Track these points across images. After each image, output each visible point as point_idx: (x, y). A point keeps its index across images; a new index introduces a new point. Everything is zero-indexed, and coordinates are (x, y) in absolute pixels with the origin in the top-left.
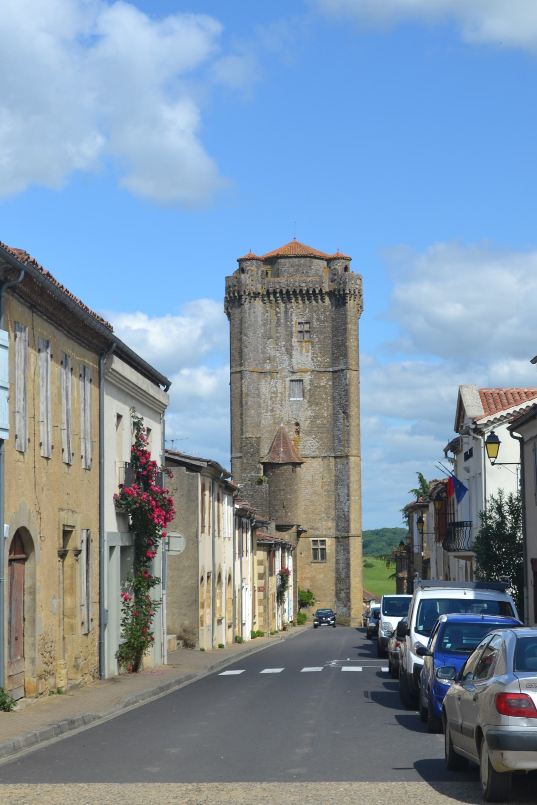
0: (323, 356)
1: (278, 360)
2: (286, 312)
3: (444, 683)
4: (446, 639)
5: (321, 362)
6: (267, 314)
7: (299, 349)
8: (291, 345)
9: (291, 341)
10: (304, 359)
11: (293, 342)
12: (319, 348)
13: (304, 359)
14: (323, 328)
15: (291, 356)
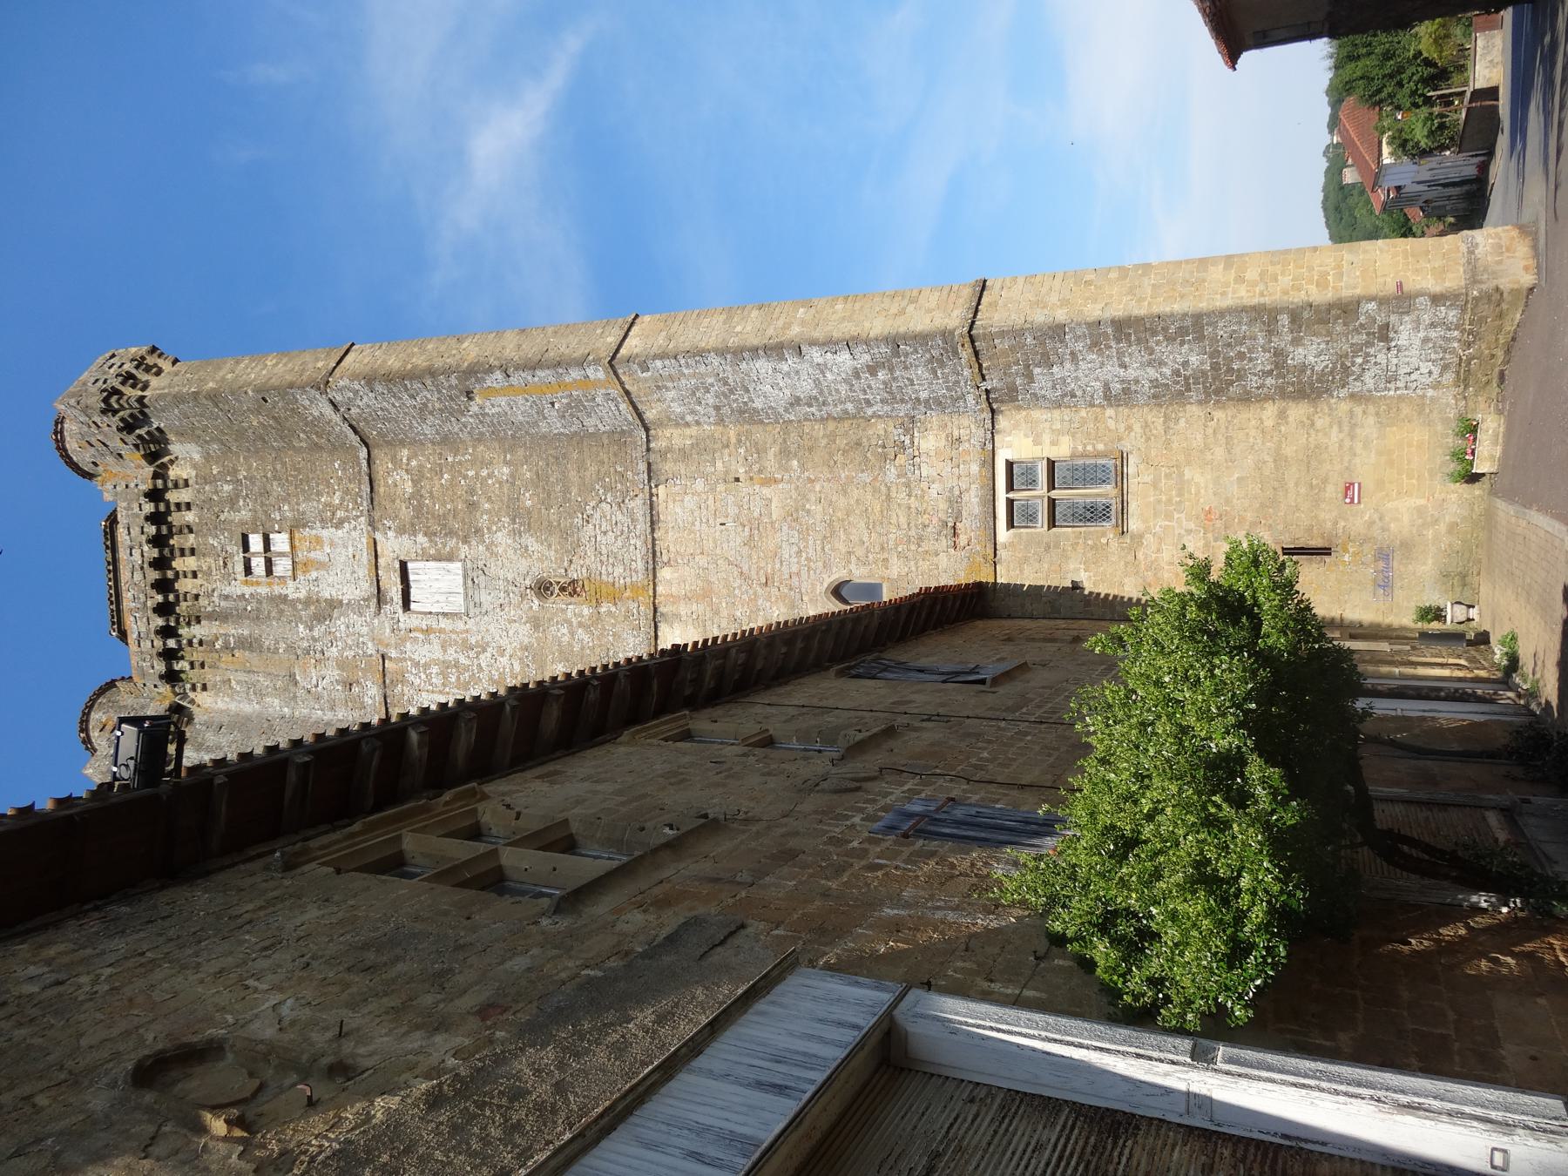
0: (328, 485)
1: (349, 654)
2: (221, 616)
5: (347, 492)
7: (314, 574)
8: (307, 602)
9: (293, 603)
10: (341, 556)
12: (308, 499)
13: (341, 556)
15: (334, 604)
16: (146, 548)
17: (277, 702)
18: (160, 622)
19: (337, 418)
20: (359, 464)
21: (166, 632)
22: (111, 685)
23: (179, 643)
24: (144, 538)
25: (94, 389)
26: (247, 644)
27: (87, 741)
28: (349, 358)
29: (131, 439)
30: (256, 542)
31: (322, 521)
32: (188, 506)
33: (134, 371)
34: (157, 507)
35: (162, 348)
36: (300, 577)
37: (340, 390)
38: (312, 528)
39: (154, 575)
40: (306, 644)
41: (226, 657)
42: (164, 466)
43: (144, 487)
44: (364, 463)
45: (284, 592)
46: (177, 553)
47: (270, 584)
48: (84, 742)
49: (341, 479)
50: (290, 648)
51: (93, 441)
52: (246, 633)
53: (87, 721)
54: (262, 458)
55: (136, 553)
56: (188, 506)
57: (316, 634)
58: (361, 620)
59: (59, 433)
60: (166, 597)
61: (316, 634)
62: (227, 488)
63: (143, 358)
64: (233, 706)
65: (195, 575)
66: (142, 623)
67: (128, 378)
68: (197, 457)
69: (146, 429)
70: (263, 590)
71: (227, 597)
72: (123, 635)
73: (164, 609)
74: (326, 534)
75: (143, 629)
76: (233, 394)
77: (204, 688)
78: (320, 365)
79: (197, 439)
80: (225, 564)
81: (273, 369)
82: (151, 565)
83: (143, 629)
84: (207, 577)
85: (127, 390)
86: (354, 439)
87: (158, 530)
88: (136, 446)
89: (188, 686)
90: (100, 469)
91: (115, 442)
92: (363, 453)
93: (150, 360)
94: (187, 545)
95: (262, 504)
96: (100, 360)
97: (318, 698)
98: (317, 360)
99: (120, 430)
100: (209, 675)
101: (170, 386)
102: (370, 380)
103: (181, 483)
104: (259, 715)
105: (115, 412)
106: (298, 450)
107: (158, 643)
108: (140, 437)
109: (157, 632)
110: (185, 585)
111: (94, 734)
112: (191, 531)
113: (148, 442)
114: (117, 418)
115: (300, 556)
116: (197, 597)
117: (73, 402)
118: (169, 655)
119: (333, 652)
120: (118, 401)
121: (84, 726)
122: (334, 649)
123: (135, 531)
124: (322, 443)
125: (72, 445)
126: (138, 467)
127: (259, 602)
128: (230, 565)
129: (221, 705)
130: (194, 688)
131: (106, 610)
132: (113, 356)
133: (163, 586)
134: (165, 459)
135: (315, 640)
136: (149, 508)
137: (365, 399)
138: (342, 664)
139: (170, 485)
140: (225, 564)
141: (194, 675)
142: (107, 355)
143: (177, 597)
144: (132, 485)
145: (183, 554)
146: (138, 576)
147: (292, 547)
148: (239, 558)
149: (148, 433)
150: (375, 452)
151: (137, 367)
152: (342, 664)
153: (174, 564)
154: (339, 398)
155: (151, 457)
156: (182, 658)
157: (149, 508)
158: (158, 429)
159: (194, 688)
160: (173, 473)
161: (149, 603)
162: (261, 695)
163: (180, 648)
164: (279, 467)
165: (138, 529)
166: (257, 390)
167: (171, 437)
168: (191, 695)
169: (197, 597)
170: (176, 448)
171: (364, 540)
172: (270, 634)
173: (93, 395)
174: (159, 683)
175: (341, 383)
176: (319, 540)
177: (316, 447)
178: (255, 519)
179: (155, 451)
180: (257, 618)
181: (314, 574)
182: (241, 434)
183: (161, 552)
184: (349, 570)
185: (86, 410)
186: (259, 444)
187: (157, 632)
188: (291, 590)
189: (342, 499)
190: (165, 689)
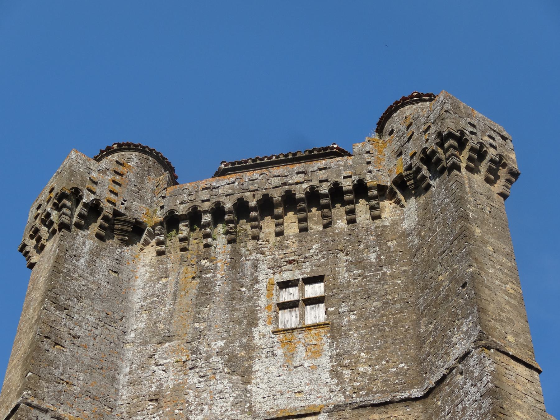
0: (379, 359)
1: (191, 396)
2: (235, 263)
3: (253, 205)
4: (411, 185)
5: (372, 379)
6: (164, 281)
7: (279, 352)
8: (249, 348)
9: (248, 333)
10: (300, 379)
11: (257, 336)
12: (362, 338)
13: (300, 379)
14: (378, 282)
15: (246, 375)
16: (305, 186)
17: (142, 325)
18: (228, 205)
19: (451, 361)
20: (404, 390)
21: (218, 213)
22: (165, 164)
23: (207, 225)
24: (316, 183)
25: (463, 124)
26: (205, 293)
27: (109, 151)
28: (521, 369)
29: (416, 162)
30: (314, 290)
31: (339, 356)
32: (351, 222)
33: (488, 158)
34: (348, 192)
35: (518, 183)
36: (276, 338)
37: (480, 362)
38: (330, 346)
39: (277, 195)
40: (203, 349)
41: (192, 271)
42: (392, 196)
43: (368, 178)
44: (405, 395)
45: (261, 323)
46: (302, 215)
47: (269, 307)
48: (108, 148)
49: (386, 371)
50: (199, 334)
51: (412, 128)
52: (217, 289)
53: (129, 149)
54: (406, 289)
55: (300, 178)
56: (351, 222)
57: (214, 359)
58: (227, 404)
59: (421, 98)
60: (254, 209)
61: (214, 359)
62: (373, 257)
63: (504, 165)
64: (139, 282)
65: (278, 234)
66: (227, 190)
67: (480, 154)
68: (405, 225)
69: (428, 175)
70: (262, 301)
71: (255, 266)
72: (221, 173)
73: (242, 209)
74: (325, 360)
75: (221, 191)
76: (468, 253)
77: (160, 253)
78: (511, 338)
79: (422, 223)
80: (291, 262)
81: (501, 289)
82: (288, 192)
83: (221, 191)
84: (276, 247)
85: (466, 154)
86: (431, 382)
87: (325, 196)
88: (409, 168)
89: (162, 238)
90: (387, 138)
91: (411, 148)
92: (416, 393)
93: (503, 173)
94: (311, 224)
95: (355, 293)
96: (498, 127)
97: (143, 367)
98: (516, 335)
99: (424, 151)
100: (173, 257)
101: (474, 192)
102: (495, 393)
103: (376, 213)
104: (128, 309)
105: (441, 145)
106: (416, 324)
107: (206, 206)
108: (419, 170)
109: (218, 204)
110: (268, 226)
111: (116, 157)
112: (325, 226)
113: (415, 178)
114: (435, 147)
115: (299, 336)
116: (256, 238)
117: (448, 106)
118: (194, 218)
119: (193, 378)
120: (451, 146)
121: (121, 147)
122: (196, 379)
123: (323, 175)
124: (425, 349)
125: (408, 110)
126: (390, 171)
127: (250, 299)
128: (289, 267)
129: (141, 270)
130: (159, 243)
131: (247, 155)
132: (504, 138)
133: (266, 206)
134: (400, 196)
135: (207, 359)
136: (347, 185)
137: (473, 390)
138: (179, 389)
139: (373, 202)
140: (291, 262)
141: (174, 242)
142: (505, 133)
143: (255, 219)
144: (370, 167)
145: (300, 221)
146: (276, 181)
147: (310, 327)
148: (298, 275)
149: (424, 177)
150: (419, 406)
151: (492, 161)
152: (179, 389)
153: (291, 214)
154: (472, 361)
155: (400, 183)
156: (192, 230)
157: (347, 185)
158: (429, 186)
159: (159, 243)
160: (387, 205)
161: (248, 194)
162: (150, 309)
163: (202, 227)
164: (398, 306)
165: (324, 177)
166: (473, 277)
167: (422, 199)
168: (153, 242)
169: (256, 238)
170: (412, 205)
171: (318, 402)
172: (216, 313)
173: (456, 124)
174: (165, 210)
175: (488, 363)
176: (317, 353)
177: (421, 342)
178: (340, 287)
179: (408, 185)
180: (233, 297)
181: (279, 352)
182: (429, 265)
183: (301, 200)
184: (284, 388)
185: (440, 118)
186: (421, 284)
187: (218, 204)
188: (262, 334)
189: (363, 375)
190: (159, 216)
